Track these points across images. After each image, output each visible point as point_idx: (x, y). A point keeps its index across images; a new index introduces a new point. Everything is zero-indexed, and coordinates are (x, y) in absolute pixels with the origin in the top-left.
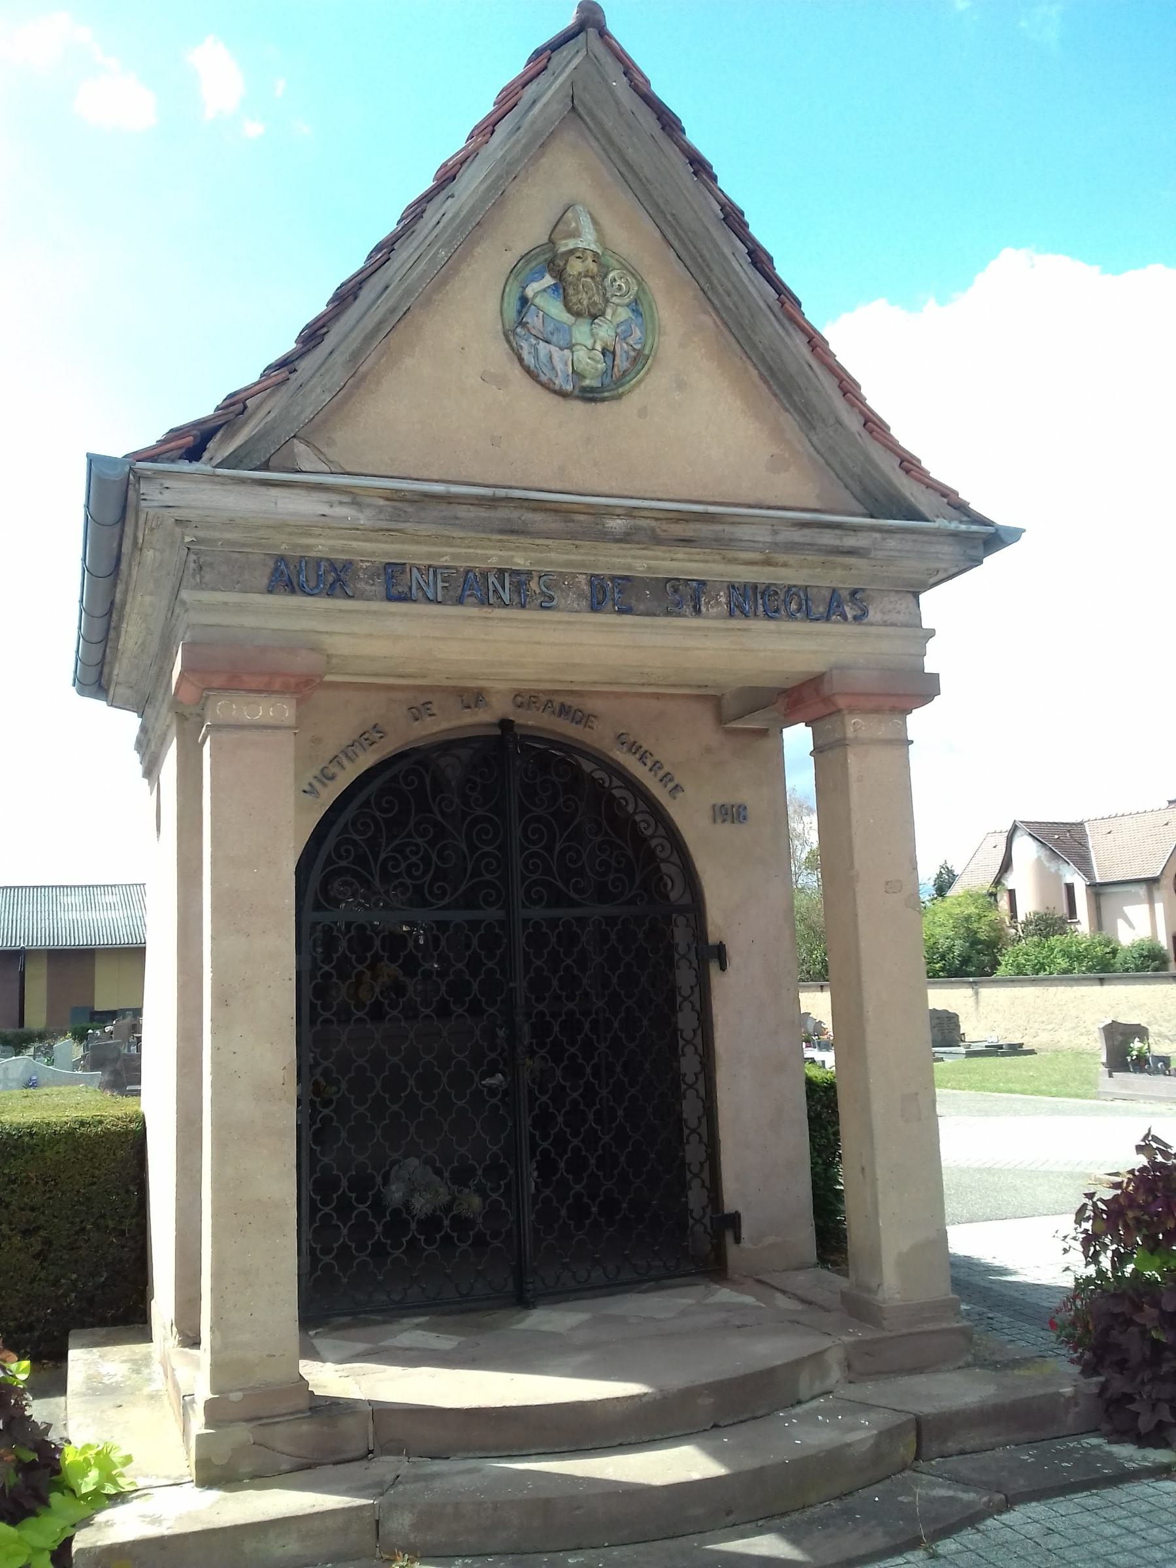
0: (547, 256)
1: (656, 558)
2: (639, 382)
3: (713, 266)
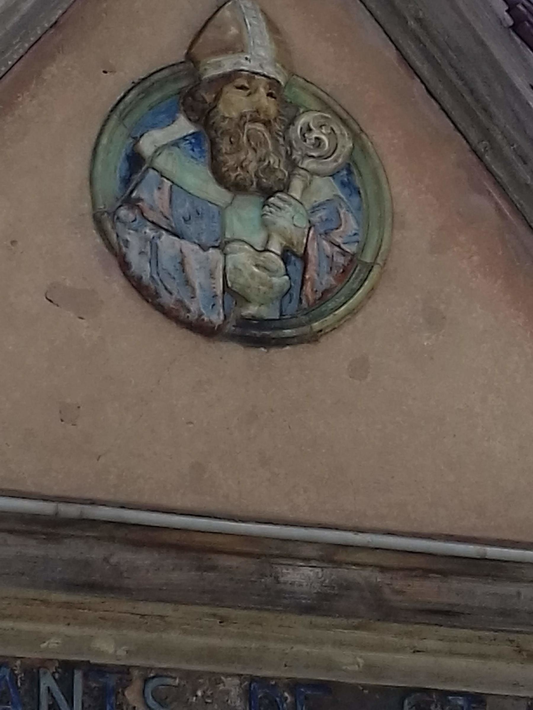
0: (183, 84)
1: (382, 648)
2: (353, 312)
3: (493, 109)
